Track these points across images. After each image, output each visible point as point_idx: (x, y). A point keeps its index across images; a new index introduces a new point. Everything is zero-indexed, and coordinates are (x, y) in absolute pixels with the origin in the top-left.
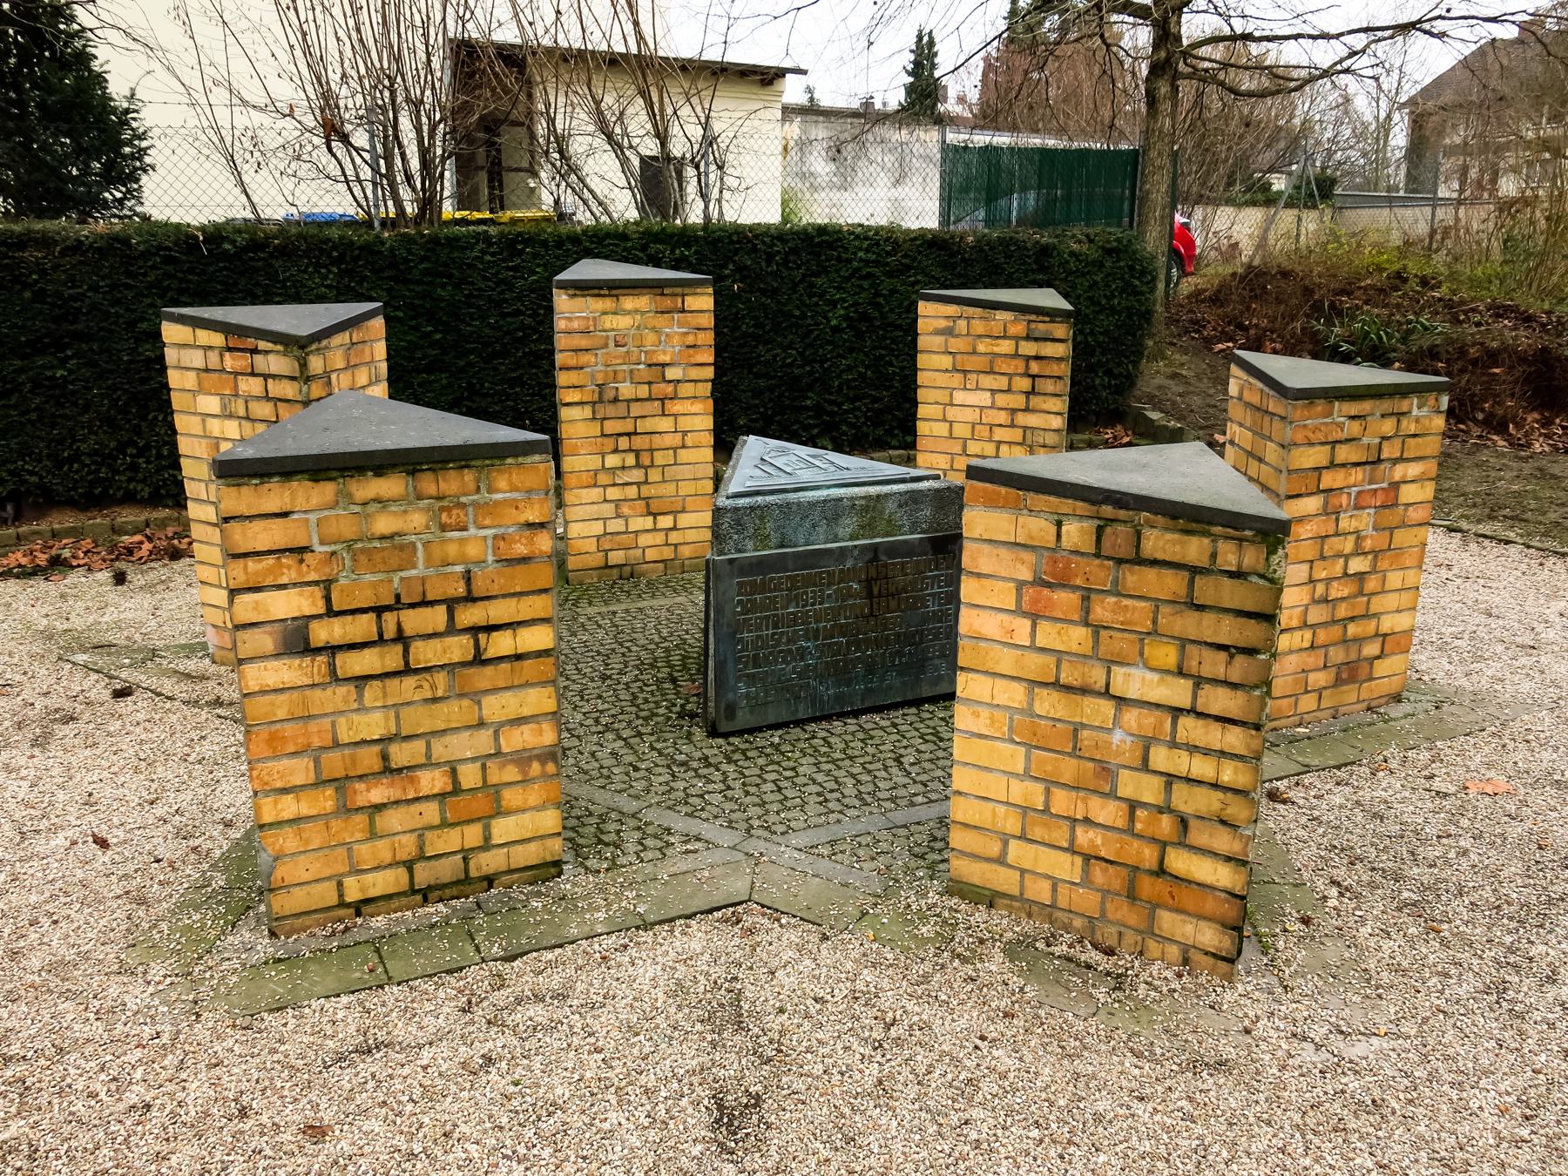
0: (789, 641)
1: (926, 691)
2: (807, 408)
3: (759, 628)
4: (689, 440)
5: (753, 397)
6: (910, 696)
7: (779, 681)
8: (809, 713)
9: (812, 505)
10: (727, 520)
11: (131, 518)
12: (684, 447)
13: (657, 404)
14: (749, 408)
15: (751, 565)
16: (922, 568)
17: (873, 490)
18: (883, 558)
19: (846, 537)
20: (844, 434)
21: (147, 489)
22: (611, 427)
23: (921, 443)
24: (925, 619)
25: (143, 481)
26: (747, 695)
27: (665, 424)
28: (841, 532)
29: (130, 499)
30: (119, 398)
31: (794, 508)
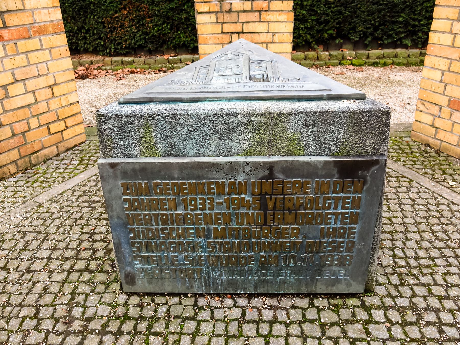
0: (179, 237)
1: (320, 288)
2: (400, 23)
3: (148, 222)
4: (276, 38)
5: (368, 15)
6: (304, 290)
7: (172, 264)
8: (204, 290)
9: (202, 118)
10: (110, 126)
11: (87, 59)
12: (273, 42)
13: (257, 14)
14: (365, 21)
15: (134, 170)
16: (325, 188)
17: (274, 107)
18: (280, 176)
19: (240, 154)
20: (419, 38)
21: (91, 48)
22: (228, 28)
23: (430, 49)
24: (323, 234)
25: (90, 44)
26: (143, 270)
27: (262, 27)
28: (235, 147)
29: (86, 51)
30: (75, 8)
31: (182, 119)
